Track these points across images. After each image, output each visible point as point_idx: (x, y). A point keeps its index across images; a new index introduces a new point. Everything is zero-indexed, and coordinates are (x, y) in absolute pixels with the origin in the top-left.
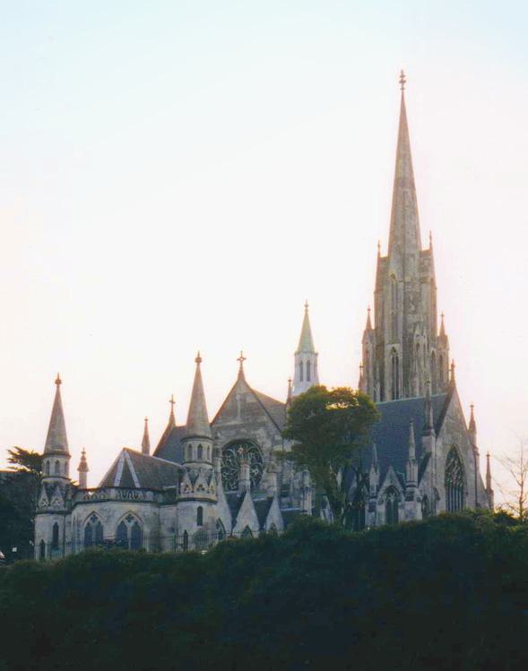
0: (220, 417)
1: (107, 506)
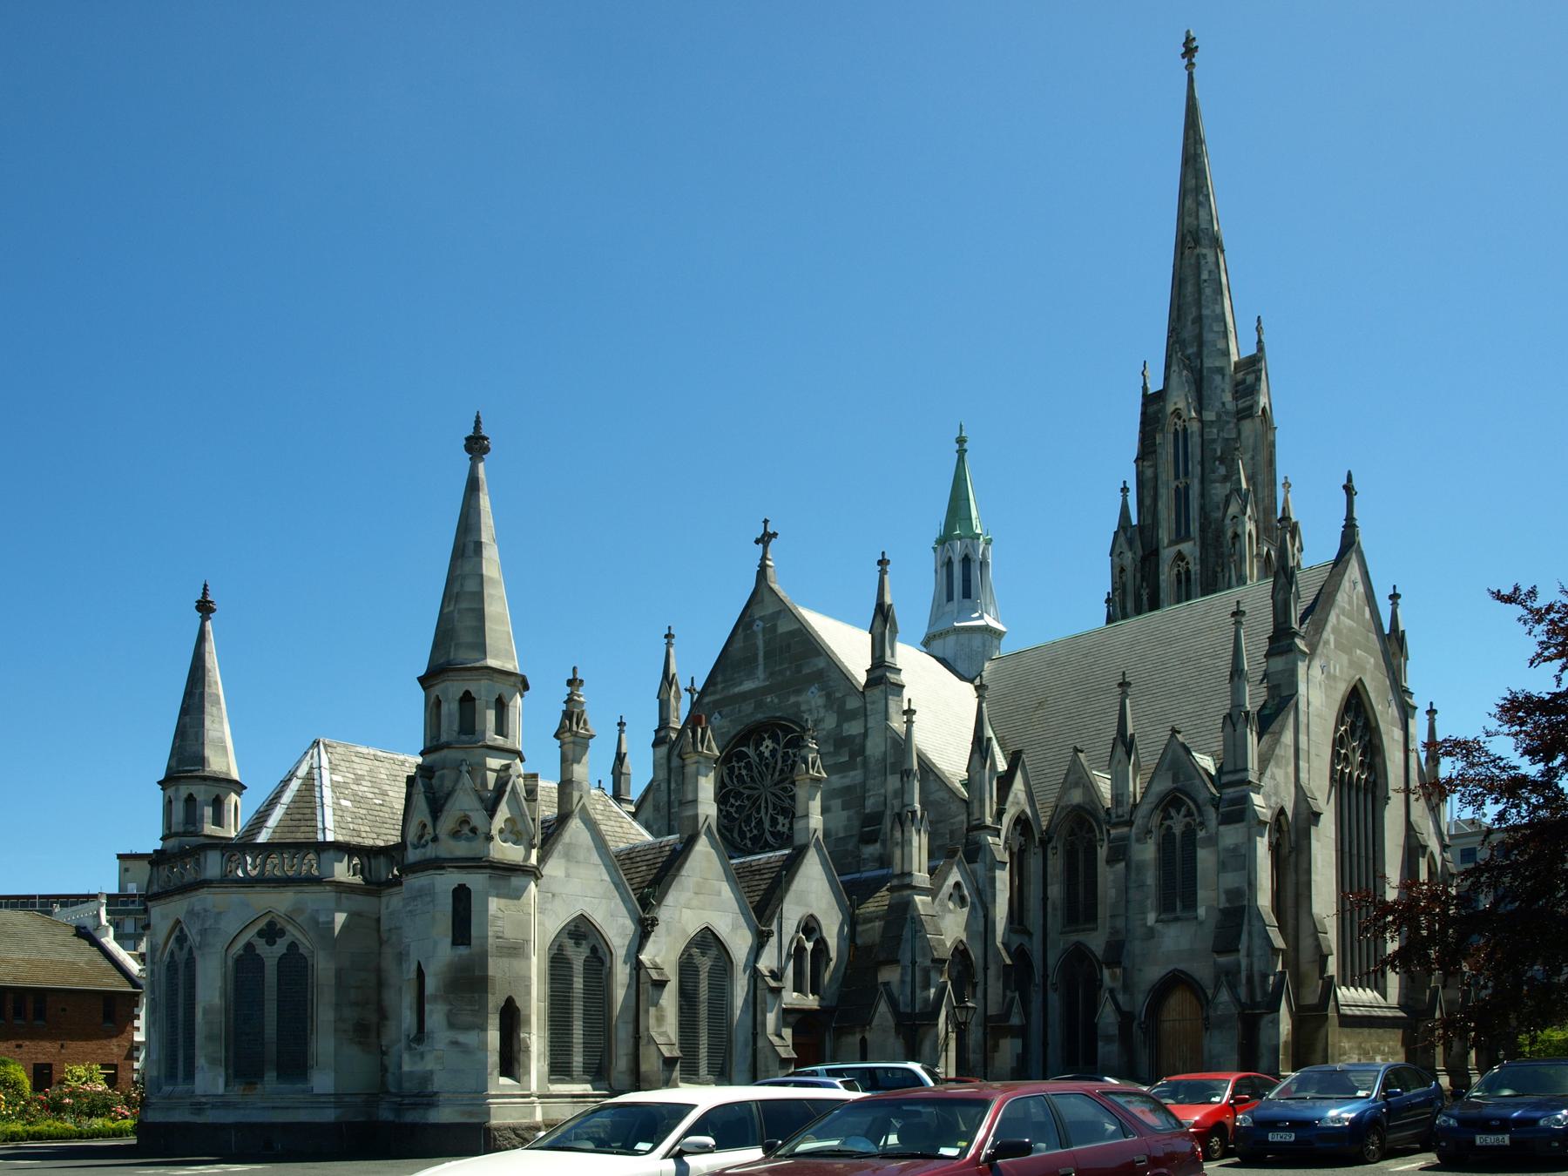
0: (719, 679)
1: (206, 899)
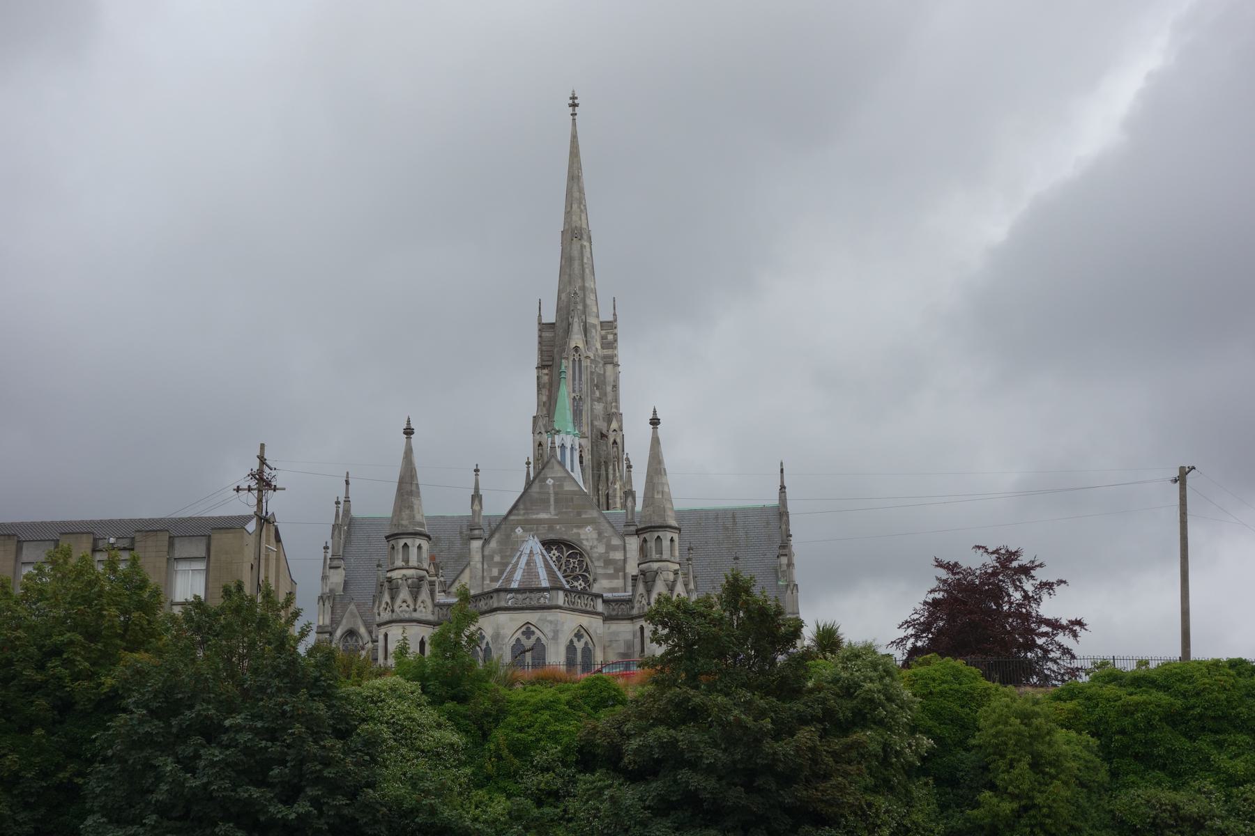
0: (521, 506)
1: (550, 615)
